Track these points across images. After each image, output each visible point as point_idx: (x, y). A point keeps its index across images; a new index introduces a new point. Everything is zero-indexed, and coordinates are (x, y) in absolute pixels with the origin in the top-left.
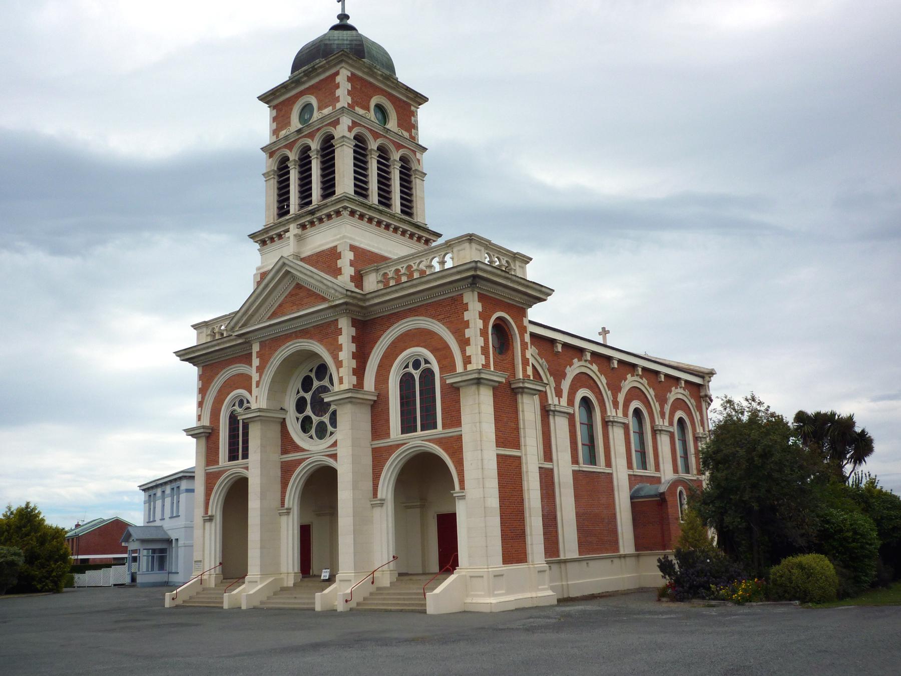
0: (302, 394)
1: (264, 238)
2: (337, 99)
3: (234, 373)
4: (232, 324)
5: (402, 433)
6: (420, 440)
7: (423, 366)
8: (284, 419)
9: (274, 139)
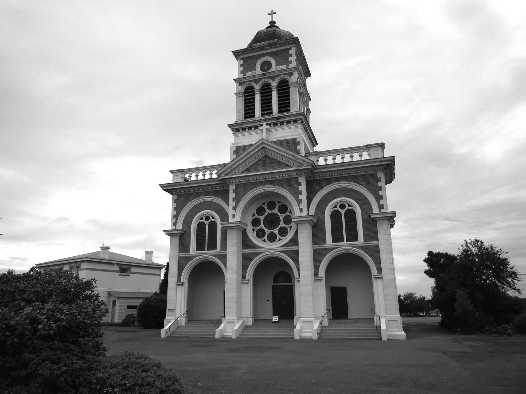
0: (257, 216)
1: (236, 128)
2: (291, 62)
3: (204, 201)
4: (220, 172)
5: (333, 242)
6: (206, 254)
7: (211, 219)
8: (245, 229)
9: (242, 76)
